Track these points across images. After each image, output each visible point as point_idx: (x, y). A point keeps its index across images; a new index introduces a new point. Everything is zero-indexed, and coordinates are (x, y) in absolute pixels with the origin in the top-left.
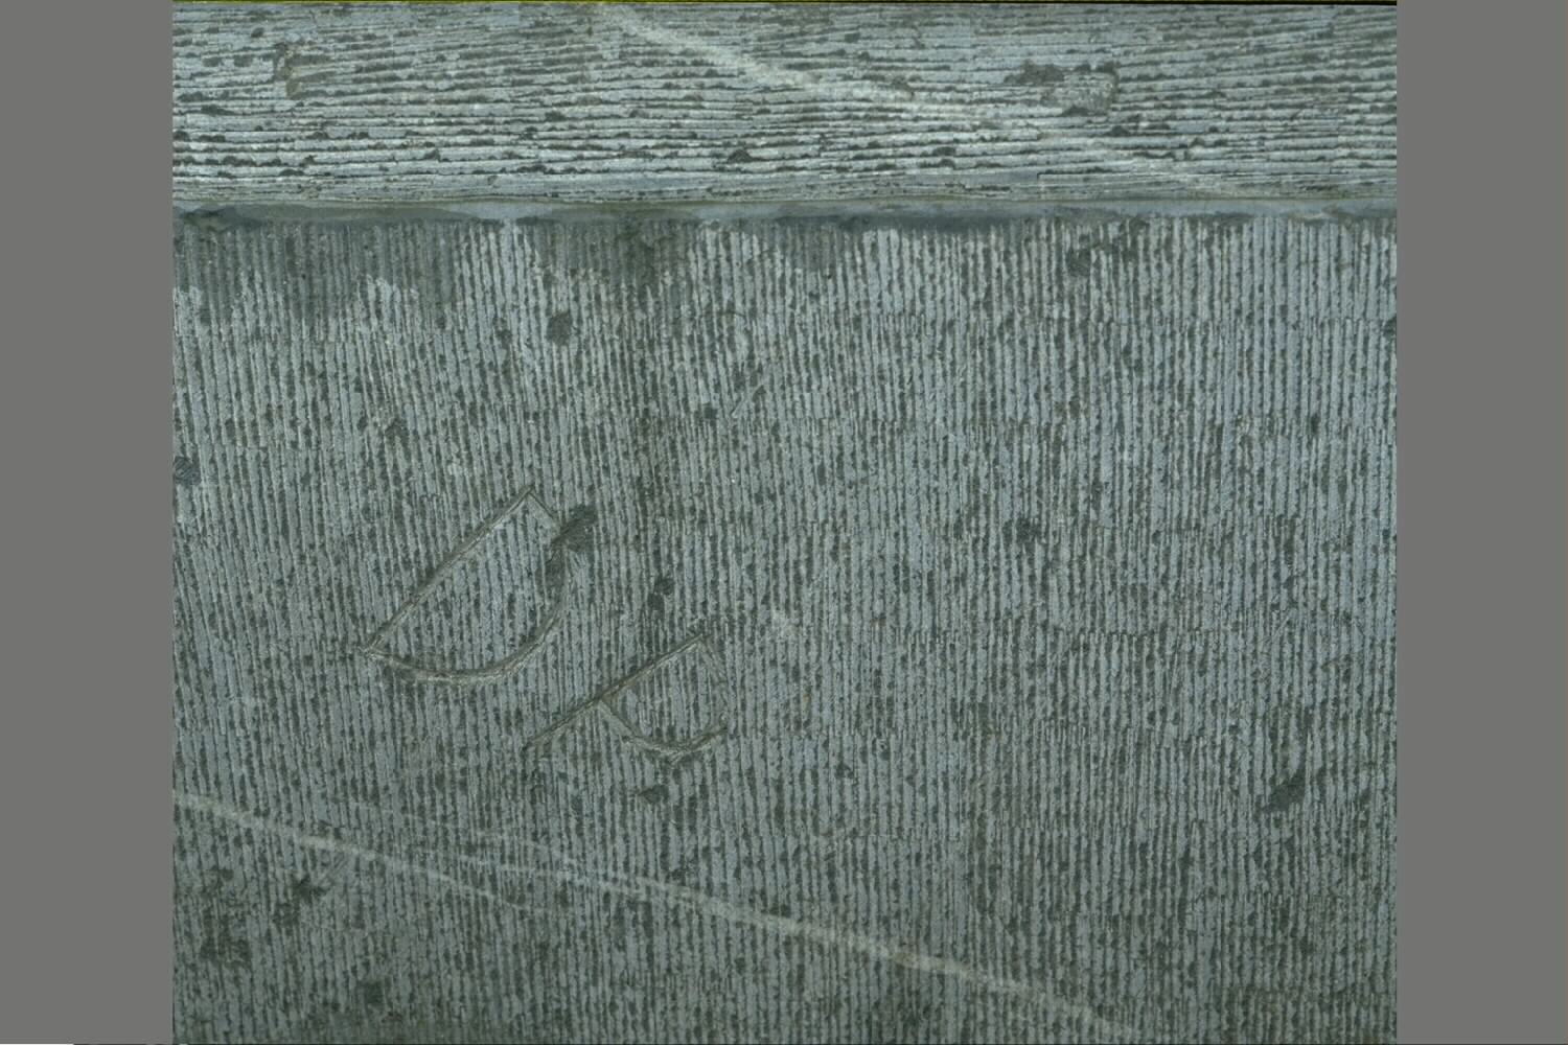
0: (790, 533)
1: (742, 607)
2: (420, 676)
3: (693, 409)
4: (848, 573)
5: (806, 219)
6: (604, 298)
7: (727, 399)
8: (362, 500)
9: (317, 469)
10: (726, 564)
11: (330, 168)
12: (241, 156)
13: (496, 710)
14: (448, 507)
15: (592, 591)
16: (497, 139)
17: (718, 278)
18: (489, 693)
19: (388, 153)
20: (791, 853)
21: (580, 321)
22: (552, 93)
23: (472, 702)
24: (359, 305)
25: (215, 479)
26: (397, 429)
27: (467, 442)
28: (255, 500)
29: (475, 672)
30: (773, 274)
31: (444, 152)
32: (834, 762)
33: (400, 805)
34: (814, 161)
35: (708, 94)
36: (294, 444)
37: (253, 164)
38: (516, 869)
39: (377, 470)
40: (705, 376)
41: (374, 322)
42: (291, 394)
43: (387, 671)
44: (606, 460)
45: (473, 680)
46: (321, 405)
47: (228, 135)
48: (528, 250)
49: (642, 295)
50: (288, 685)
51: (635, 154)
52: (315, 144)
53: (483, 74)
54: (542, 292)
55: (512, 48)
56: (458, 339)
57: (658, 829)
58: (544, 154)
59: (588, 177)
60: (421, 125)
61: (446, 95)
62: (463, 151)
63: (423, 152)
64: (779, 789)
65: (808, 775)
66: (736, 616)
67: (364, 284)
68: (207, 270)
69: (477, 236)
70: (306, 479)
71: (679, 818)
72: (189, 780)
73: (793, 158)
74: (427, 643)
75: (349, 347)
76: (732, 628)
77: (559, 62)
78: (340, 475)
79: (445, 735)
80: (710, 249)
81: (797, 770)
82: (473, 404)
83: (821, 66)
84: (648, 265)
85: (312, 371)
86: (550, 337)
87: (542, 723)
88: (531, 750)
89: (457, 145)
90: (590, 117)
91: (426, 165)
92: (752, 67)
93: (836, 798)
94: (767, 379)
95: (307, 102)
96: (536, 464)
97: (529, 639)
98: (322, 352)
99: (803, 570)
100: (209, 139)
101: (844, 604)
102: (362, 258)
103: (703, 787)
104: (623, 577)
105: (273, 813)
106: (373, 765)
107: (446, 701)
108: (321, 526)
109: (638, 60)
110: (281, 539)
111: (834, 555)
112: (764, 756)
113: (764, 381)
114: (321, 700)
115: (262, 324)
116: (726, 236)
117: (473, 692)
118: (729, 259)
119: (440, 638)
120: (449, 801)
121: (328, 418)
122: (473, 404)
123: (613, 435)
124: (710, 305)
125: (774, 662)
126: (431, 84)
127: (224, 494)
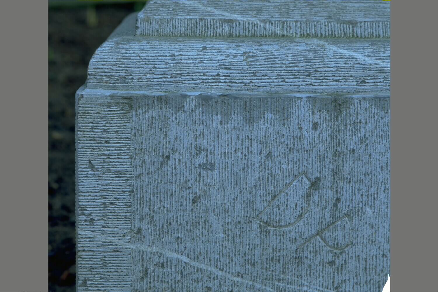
0: (373, 185)
1: (359, 207)
2: (269, 228)
3: (349, 149)
4: (388, 197)
5: (381, 97)
6: (327, 118)
7: (358, 147)
8: (258, 175)
9: (247, 166)
10: (355, 194)
11: (256, 84)
12: (233, 81)
13: (290, 238)
14: (281, 177)
15: (318, 202)
16: (301, 77)
17: (358, 113)
18: (288, 232)
19: (272, 80)
20: (368, 280)
21: (320, 124)
22: (315, 65)
23: (283, 235)
24: (262, 120)
25: (219, 169)
26: (269, 155)
27: (288, 159)
28: (230, 175)
29: (284, 226)
30: (372, 112)
31: (287, 80)
32: (382, 253)
33: (261, 267)
34: (382, 83)
35: (356, 65)
36: (242, 159)
37: (236, 83)
38: (292, 287)
39: (263, 166)
40: (353, 140)
41: (266, 124)
42: (242, 145)
43: (260, 226)
44: (325, 164)
45: (284, 229)
46: (250, 148)
47: (231, 75)
48: (308, 105)
49: (337, 117)
50: (233, 230)
51: (336, 81)
52: (253, 78)
53: (298, 60)
54: (311, 116)
55: (305, 54)
56: (288, 129)
57: (332, 274)
58: (313, 81)
59: (324, 87)
60: (281, 73)
61: (288, 65)
62: (292, 80)
63: (281, 80)
64: (366, 261)
65: (374, 257)
66: (357, 209)
67: (264, 114)
68: (223, 110)
69: (295, 101)
70: (243, 169)
71: (338, 270)
72: (202, 259)
73: (377, 82)
74: (272, 218)
75: (259, 131)
76: (356, 213)
77: (317, 57)
78: (253, 168)
79: (275, 245)
80: (356, 105)
81: (371, 256)
82: (290, 148)
83: (384, 59)
84: (339, 110)
85: (248, 138)
86: (312, 129)
87: (302, 242)
88: (298, 250)
89: (290, 78)
90: (325, 71)
91: (281, 84)
92: (367, 59)
93: (382, 264)
94: (369, 141)
95: (251, 67)
96: (306, 165)
97: (300, 216)
98: (252, 133)
99: (376, 195)
100: (225, 76)
101: (386, 206)
102: (264, 106)
103: (345, 261)
104: (327, 198)
105: (225, 269)
106: (254, 255)
107: (276, 235)
108: (246, 183)
109: (338, 57)
110: (235, 186)
111: (384, 191)
112: (362, 251)
113: (368, 142)
114: (242, 235)
115: (236, 125)
116: (360, 101)
117: (284, 232)
118: (361, 108)
119: (276, 216)
120: (274, 266)
121: (251, 152)
122: (290, 148)
123: (327, 157)
124: (355, 120)
125: (366, 223)
126: (284, 62)
127: (221, 173)
